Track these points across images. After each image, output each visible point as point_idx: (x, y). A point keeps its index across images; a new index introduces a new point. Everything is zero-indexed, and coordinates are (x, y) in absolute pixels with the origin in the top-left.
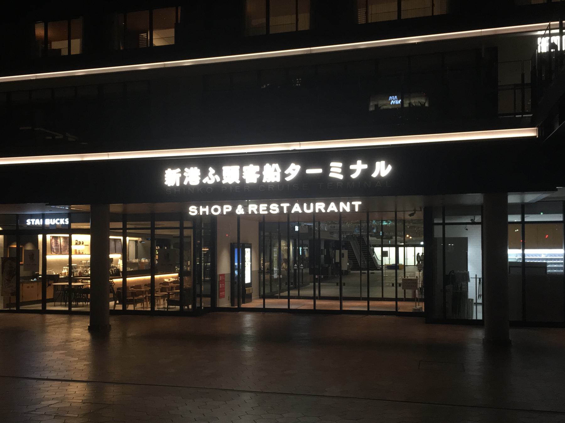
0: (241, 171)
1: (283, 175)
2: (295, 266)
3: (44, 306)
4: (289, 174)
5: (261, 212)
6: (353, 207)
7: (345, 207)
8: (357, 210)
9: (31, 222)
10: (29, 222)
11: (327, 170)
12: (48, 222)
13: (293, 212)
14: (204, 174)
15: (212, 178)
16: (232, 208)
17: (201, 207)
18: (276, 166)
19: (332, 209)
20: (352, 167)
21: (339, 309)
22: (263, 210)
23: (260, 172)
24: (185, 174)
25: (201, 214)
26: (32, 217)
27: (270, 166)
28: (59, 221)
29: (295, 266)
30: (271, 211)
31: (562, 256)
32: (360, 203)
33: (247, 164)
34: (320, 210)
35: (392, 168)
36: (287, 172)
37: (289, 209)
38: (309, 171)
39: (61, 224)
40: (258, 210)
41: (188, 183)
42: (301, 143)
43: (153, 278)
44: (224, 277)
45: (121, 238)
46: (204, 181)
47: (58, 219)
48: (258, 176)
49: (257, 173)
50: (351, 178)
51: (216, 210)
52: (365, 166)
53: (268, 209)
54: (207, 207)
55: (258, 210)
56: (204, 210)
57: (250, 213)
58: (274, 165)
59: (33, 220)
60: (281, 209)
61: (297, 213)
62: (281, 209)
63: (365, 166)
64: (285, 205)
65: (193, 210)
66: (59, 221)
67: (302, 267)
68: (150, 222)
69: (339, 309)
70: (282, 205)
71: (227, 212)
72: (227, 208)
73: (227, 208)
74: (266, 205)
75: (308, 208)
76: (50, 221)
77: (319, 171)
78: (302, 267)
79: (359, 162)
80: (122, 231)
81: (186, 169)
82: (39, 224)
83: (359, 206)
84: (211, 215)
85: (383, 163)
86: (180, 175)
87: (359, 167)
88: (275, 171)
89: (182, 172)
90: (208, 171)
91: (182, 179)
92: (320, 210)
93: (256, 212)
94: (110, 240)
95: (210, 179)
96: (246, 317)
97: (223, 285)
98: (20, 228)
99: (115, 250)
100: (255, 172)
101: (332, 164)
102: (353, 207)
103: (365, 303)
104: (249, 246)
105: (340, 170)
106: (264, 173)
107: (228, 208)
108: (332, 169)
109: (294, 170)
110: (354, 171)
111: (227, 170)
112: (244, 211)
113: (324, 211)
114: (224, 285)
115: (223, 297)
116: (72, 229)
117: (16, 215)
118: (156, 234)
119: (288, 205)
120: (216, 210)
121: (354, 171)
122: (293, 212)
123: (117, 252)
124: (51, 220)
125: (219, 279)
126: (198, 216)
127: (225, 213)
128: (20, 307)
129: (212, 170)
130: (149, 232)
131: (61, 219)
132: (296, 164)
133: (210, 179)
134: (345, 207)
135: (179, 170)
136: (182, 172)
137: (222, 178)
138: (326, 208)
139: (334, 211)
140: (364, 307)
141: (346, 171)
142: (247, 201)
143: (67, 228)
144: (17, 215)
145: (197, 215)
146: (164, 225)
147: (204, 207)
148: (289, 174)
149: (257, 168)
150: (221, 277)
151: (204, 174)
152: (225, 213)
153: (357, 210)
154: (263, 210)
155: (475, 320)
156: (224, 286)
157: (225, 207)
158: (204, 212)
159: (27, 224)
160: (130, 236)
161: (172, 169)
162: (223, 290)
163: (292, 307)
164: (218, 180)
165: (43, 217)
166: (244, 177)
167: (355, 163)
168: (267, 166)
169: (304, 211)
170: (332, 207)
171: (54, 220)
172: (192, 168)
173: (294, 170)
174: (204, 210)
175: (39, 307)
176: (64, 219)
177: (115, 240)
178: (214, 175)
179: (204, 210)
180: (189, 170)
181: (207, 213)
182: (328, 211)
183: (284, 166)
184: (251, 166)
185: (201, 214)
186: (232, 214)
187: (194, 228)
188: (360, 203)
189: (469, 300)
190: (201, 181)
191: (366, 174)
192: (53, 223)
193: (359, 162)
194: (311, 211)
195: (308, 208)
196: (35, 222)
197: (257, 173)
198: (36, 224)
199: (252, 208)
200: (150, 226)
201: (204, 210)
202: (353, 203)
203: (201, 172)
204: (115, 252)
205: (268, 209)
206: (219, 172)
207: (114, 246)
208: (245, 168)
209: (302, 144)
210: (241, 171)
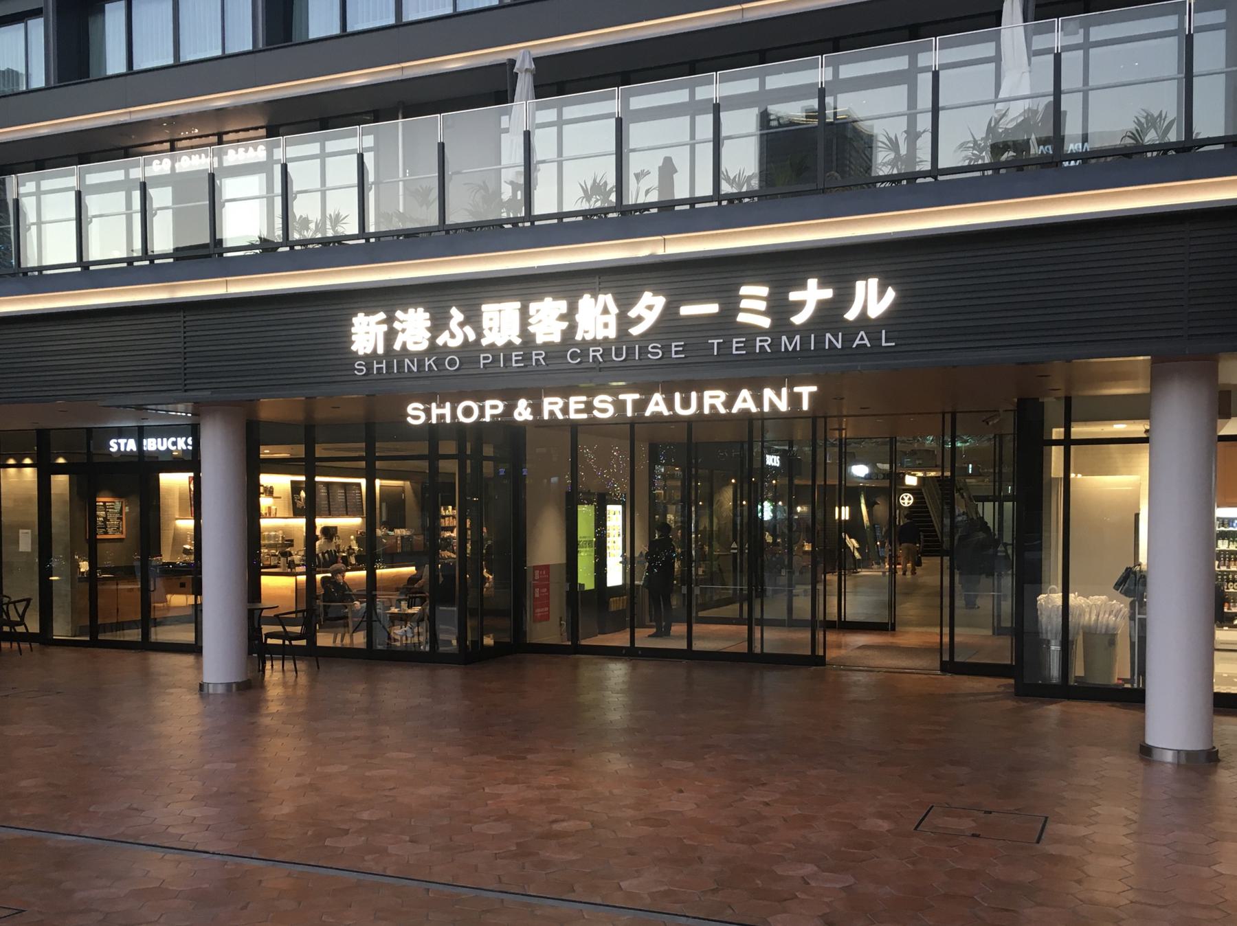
0: (524, 314)
1: (624, 322)
2: (732, 546)
3: (146, 634)
4: (639, 319)
5: (573, 416)
6: (795, 399)
8: (805, 406)
9: (119, 444)
10: (113, 445)
11: (731, 306)
13: (648, 413)
14: (439, 324)
15: (456, 335)
18: (607, 299)
19: (745, 406)
20: (794, 296)
21: (810, 653)
22: (578, 411)
23: (569, 316)
25: (706, 411)
28: (175, 444)
29: (732, 546)
32: (814, 389)
33: (539, 297)
35: (896, 294)
36: (632, 314)
37: (640, 405)
38: (686, 310)
39: (179, 448)
40: (565, 410)
41: (404, 345)
42: (666, 237)
43: (371, 575)
44: (548, 573)
45: (363, 482)
46: (440, 341)
47: (173, 439)
48: (564, 325)
50: (847, 321)
51: (468, 412)
52: (828, 293)
53: (589, 407)
54: (448, 405)
55: (565, 410)
56: (441, 412)
58: (601, 297)
60: (620, 406)
61: (657, 417)
62: (620, 406)
63: (828, 293)
67: (735, 549)
68: (363, 445)
69: (810, 653)
71: (493, 416)
72: (493, 408)
73: (493, 408)
75: (686, 404)
76: (157, 444)
77: (712, 308)
78: (735, 549)
79: (812, 283)
81: (399, 314)
83: (811, 395)
85: (873, 282)
86: (385, 327)
88: (606, 311)
89: (390, 320)
91: (390, 336)
93: (560, 416)
95: (453, 336)
96: (626, 674)
98: (96, 459)
99: (347, 508)
100: (557, 315)
101: (745, 290)
102: (795, 399)
103: (806, 635)
106: (578, 317)
108: (744, 304)
109: (650, 308)
110: (800, 306)
111: (490, 311)
113: (722, 410)
115: (546, 617)
116: (1042, 448)
117: (85, 430)
119: (637, 396)
120: (468, 412)
122: (648, 413)
123: (349, 513)
124: (159, 440)
125: (532, 578)
126: (427, 426)
128: (100, 635)
129: (457, 315)
130: (424, 465)
131: (179, 439)
132: (656, 292)
133: (453, 336)
134: (776, 400)
135: (382, 316)
136: (390, 320)
137: (480, 335)
138: (729, 403)
139: (661, 413)
140: (703, 637)
141: (780, 309)
144: (89, 430)
146: (325, 449)
148: (639, 319)
149: (562, 306)
150: (537, 572)
151: (439, 324)
153: (805, 406)
154: (578, 411)
155: (759, 654)
156: (547, 594)
157: (488, 403)
159: (111, 449)
160: (382, 478)
161: (367, 314)
163: (698, 645)
166: (531, 329)
167: (802, 286)
169: (676, 412)
170: (745, 401)
171: (165, 440)
172: (411, 311)
173: (650, 308)
174: (441, 411)
175: (134, 635)
176: (184, 439)
177: (327, 484)
178: (461, 325)
179: (441, 412)
180: (405, 315)
181: (448, 420)
182: (735, 410)
183: (626, 302)
184: (548, 300)
185: (434, 421)
187: (460, 456)
188: (814, 389)
190: (432, 340)
191: (829, 314)
193: (812, 283)
194: (692, 411)
195: (686, 404)
196: (126, 444)
197: (562, 317)
198: (128, 449)
199: (552, 405)
201: (441, 411)
202: (796, 389)
203: (432, 319)
204: (327, 512)
205: (589, 407)
206: (473, 318)
208: (533, 307)
209: (669, 239)
210: (524, 314)
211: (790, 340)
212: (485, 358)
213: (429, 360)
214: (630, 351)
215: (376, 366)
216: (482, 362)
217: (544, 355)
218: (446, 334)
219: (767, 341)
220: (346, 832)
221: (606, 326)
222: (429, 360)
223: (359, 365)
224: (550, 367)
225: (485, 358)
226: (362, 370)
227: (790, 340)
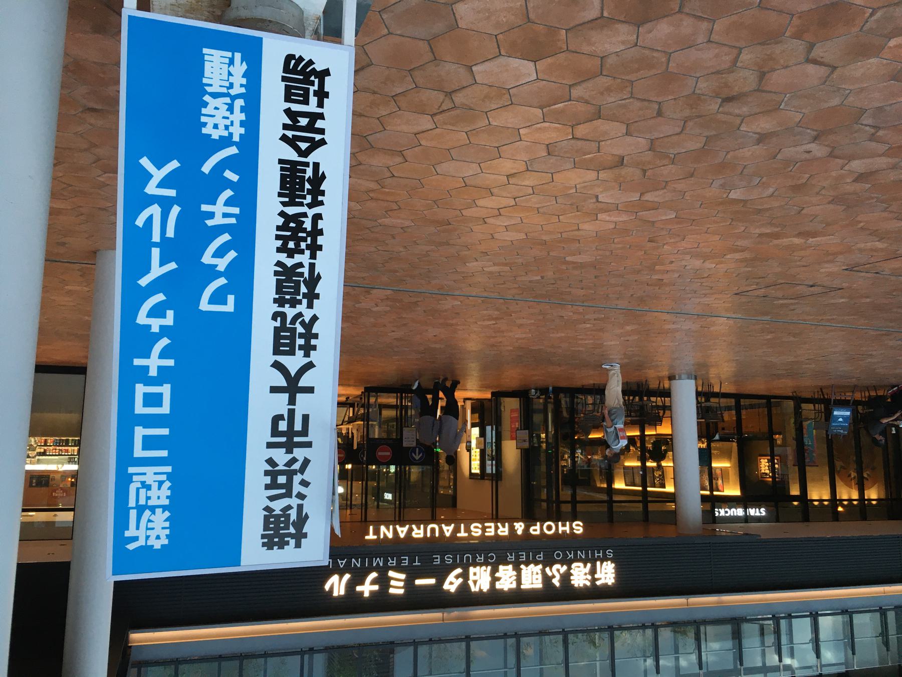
1: (465, 576)
4: (457, 577)
5: (492, 525)
6: (376, 532)
7: (386, 532)
10: (763, 512)
11: (409, 583)
12: (740, 512)
14: (566, 578)
16: (529, 530)
17: (568, 532)
20: (376, 587)
22: (490, 527)
23: (495, 580)
24: (589, 577)
26: (758, 519)
27: (482, 588)
28: (726, 512)
30: (480, 526)
31: (868, 496)
32: (367, 537)
34: (419, 528)
36: (460, 580)
37: (457, 530)
38: (432, 581)
39: (723, 510)
40: (497, 528)
46: (565, 568)
47: (727, 515)
48: (497, 575)
49: (499, 579)
52: (359, 588)
53: (484, 529)
54: (560, 532)
55: (497, 528)
56: (564, 528)
57: (507, 524)
58: (477, 589)
59: (758, 514)
60: (468, 530)
62: (468, 530)
63: (359, 588)
64: (462, 534)
65: (578, 528)
66: (726, 512)
70: (466, 535)
72: (535, 530)
73: (535, 530)
74: (486, 534)
75: (433, 530)
77: (418, 582)
80: (649, 499)
82: (750, 509)
83: (368, 534)
84: (556, 521)
87: (367, 588)
88: (475, 582)
90: (560, 581)
91: (593, 572)
92: (419, 528)
94: (640, 484)
97: (513, 426)
102: (376, 532)
104: (472, 475)
105: (393, 583)
106: (489, 579)
107: (535, 530)
108: (402, 584)
109: (451, 583)
110: (373, 582)
112: (514, 526)
114: (511, 426)
115: (512, 411)
118: (640, 496)
119: (458, 535)
120: (549, 528)
121: (373, 582)
127: (538, 524)
132: (448, 591)
133: (558, 570)
134: (386, 532)
138: (410, 530)
141: (383, 581)
142: (866, 502)
143: (716, 504)
145: (573, 521)
147: (564, 532)
148: (457, 577)
149: (498, 585)
152: (538, 524)
154: (490, 527)
157: (538, 533)
158: (564, 525)
162: (512, 420)
164: (547, 570)
165: (747, 519)
168: (486, 587)
170: (402, 531)
173: (451, 583)
174: (564, 528)
175: (743, 402)
176: (721, 515)
178: (554, 576)
179: (564, 528)
182: (407, 526)
183: (464, 587)
186: (746, 509)
189: (715, 470)
190: (570, 568)
191: (359, 578)
192: (733, 510)
193: (366, 595)
195: (433, 530)
196: (756, 512)
197: (499, 579)
200: (614, 504)
201: (564, 528)
205: (484, 529)
206: (547, 580)
207: (635, 476)
211: (378, 564)
212: (540, 557)
213: (571, 557)
214: (462, 559)
215: (601, 554)
216: (542, 555)
217: (389, 563)
218: (562, 571)
219: (509, 559)
220: (595, 319)
221: (475, 574)
222: (571, 557)
223: (610, 555)
224: (504, 551)
225: (540, 557)
226: (447, 558)
227: (378, 564)
